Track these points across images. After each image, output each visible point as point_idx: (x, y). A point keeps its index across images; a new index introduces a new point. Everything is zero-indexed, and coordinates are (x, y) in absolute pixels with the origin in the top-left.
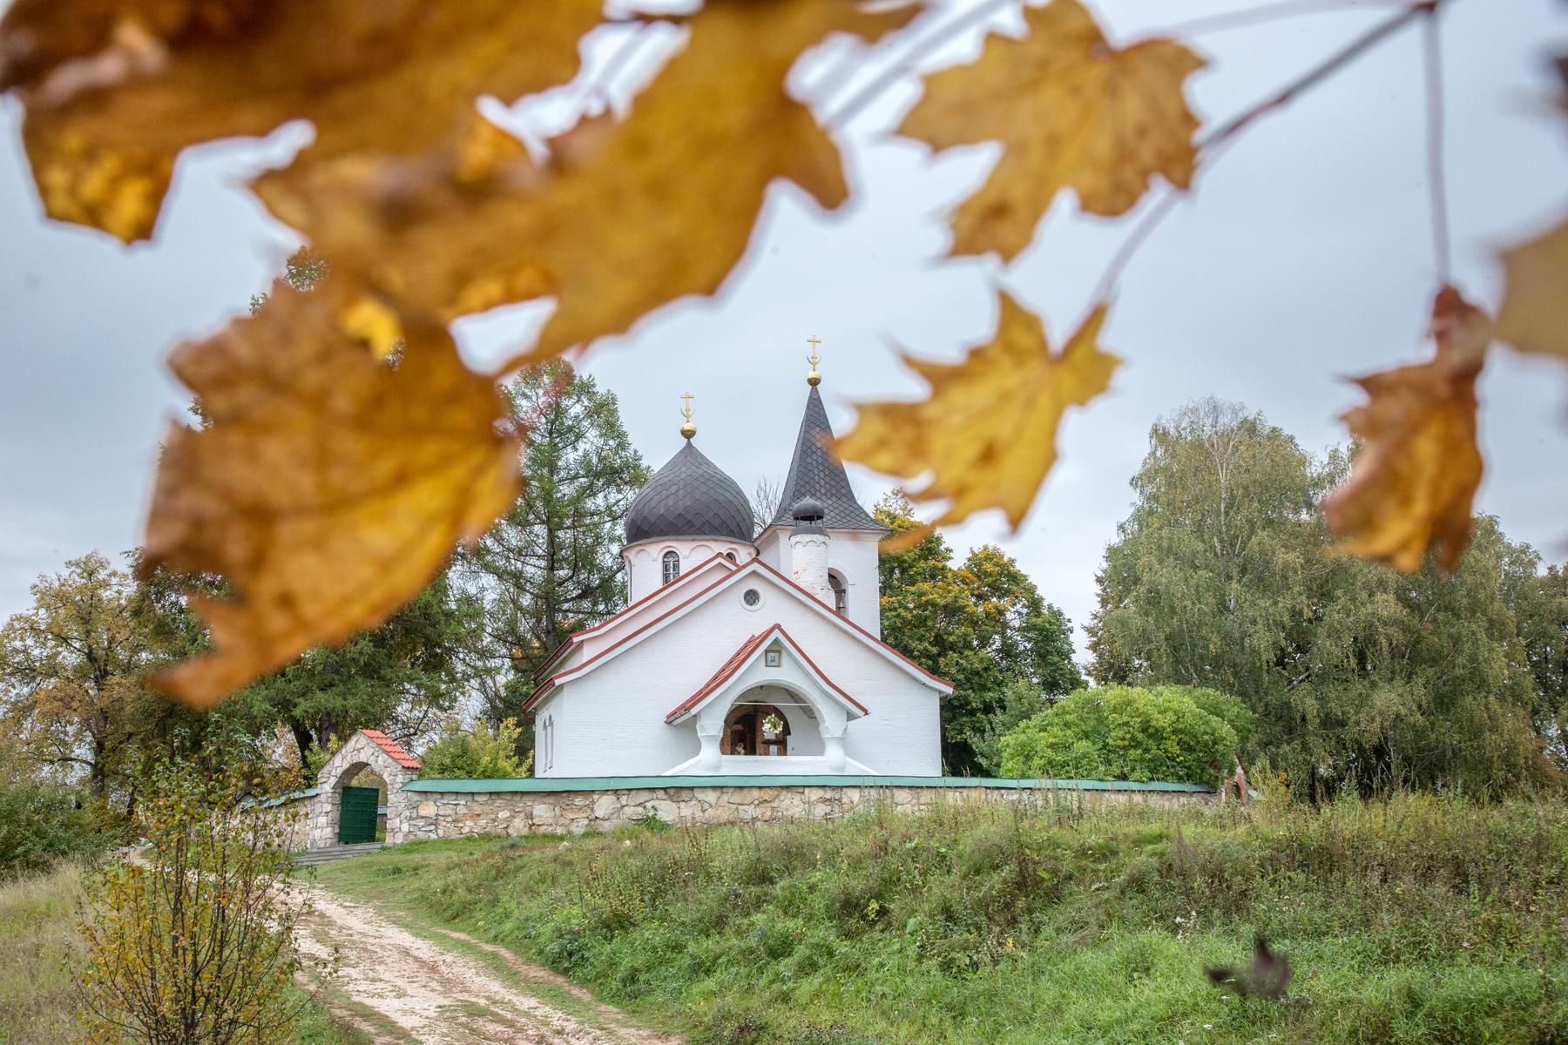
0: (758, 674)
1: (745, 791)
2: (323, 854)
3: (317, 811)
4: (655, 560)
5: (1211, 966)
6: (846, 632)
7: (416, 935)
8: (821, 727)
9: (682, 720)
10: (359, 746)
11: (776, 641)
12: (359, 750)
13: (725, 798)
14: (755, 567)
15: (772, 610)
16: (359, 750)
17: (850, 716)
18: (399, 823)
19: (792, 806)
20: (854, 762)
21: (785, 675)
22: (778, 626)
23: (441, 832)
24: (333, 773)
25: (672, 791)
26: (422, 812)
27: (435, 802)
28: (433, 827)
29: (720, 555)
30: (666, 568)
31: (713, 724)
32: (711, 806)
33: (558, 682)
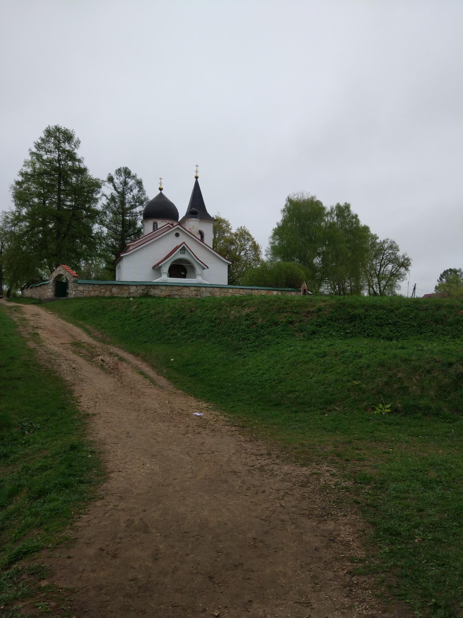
0: (178, 256)
1: (173, 287)
2: (50, 300)
3: (48, 288)
4: (151, 224)
5: (290, 197)
6: (203, 246)
7: (66, 322)
8: (195, 271)
9: (157, 268)
10: (60, 269)
11: (184, 247)
12: (60, 271)
13: (168, 288)
14: (179, 226)
15: (182, 239)
16: (60, 271)
17: (204, 269)
18: (72, 292)
19: (186, 292)
20: (204, 281)
21: (185, 256)
22: (184, 243)
23: (84, 295)
24: (53, 277)
25: (152, 286)
26: (79, 289)
27: (83, 286)
28: (82, 293)
29: (169, 223)
30: (154, 227)
31: (166, 269)
32: (163, 290)
33: (121, 255)
